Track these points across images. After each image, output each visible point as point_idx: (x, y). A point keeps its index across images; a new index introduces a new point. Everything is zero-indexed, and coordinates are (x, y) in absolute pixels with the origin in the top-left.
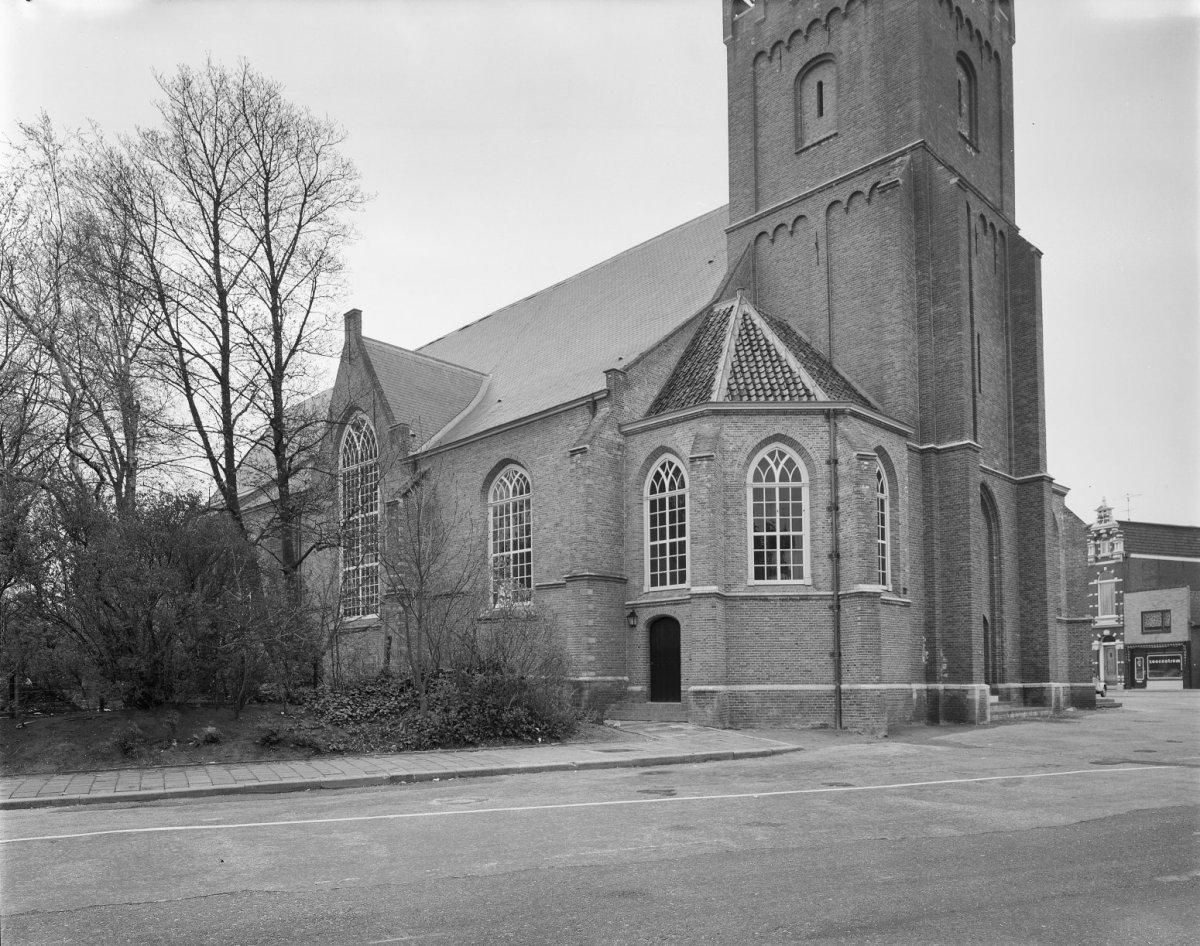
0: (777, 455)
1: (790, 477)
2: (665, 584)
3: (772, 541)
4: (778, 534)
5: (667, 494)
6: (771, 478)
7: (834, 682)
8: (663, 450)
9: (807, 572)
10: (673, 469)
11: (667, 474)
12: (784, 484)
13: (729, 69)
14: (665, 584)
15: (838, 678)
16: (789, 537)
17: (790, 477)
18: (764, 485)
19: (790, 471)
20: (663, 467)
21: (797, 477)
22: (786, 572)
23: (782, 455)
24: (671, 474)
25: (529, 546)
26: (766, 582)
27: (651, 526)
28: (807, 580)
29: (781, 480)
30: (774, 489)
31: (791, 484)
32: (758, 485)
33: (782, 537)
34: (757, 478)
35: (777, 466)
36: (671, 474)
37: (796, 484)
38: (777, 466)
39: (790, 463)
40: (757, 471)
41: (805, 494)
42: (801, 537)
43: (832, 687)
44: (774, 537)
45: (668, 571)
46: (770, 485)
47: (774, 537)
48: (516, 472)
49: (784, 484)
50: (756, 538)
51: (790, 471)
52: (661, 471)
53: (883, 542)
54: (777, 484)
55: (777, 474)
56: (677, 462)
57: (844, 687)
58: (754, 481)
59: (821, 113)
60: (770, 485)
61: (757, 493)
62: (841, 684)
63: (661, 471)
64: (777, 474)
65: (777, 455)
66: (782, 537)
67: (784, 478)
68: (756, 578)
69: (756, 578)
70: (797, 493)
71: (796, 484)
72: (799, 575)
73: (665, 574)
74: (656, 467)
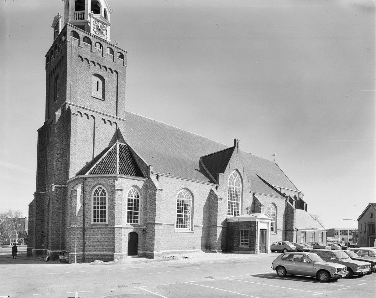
2: (99, 222)
4: (100, 210)
5: (100, 196)
6: (98, 195)
7: (83, 252)
9: (107, 220)
10: (102, 190)
11: (100, 191)
12: (102, 196)
14: (99, 222)
15: (83, 251)
18: (96, 197)
20: (98, 188)
21: (105, 195)
22: (102, 221)
23: (101, 188)
24: (101, 191)
25: (229, 202)
28: (139, 224)
29: (101, 195)
30: (99, 198)
31: (103, 196)
32: (95, 197)
33: (132, 210)
34: (95, 195)
36: (101, 191)
37: (105, 196)
39: (103, 191)
43: (82, 253)
44: (101, 209)
45: (100, 218)
46: (98, 197)
47: (101, 209)
49: (102, 196)
52: (98, 189)
53: (178, 213)
55: (100, 193)
56: (103, 188)
57: (82, 253)
59: (98, 90)
60: (98, 197)
61: (95, 199)
62: (83, 254)
63: (98, 189)
64: (100, 193)
65: (100, 188)
66: (132, 210)
67: (102, 195)
68: (94, 222)
71: (105, 196)
73: (134, 219)
74: (96, 188)
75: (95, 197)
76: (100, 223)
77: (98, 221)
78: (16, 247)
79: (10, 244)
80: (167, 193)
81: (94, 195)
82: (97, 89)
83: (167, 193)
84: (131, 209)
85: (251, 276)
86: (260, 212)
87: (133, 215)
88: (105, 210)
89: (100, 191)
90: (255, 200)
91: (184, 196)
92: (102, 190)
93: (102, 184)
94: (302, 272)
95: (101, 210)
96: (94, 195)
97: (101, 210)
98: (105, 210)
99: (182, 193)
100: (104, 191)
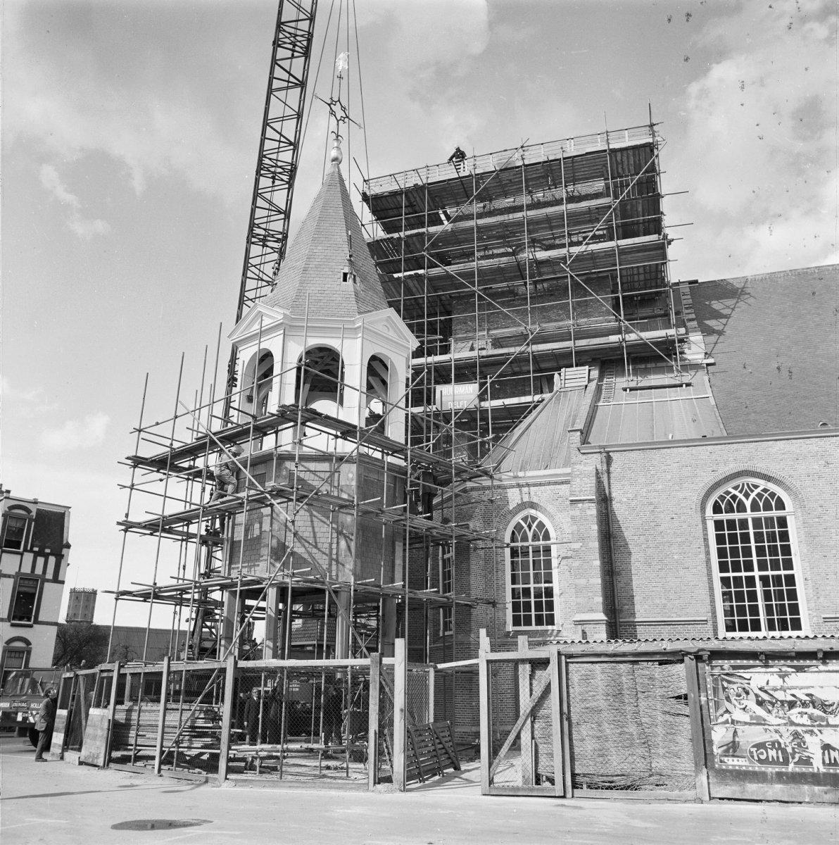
0: (529, 519)
2: (531, 625)
3: (526, 592)
6: (525, 539)
8: (533, 505)
10: (536, 523)
11: (530, 527)
12: (757, 514)
14: (531, 625)
16: (745, 571)
19: (519, 533)
20: (525, 519)
21: (547, 537)
27: (787, 532)
28: (806, 630)
29: (533, 540)
30: (746, 520)
32: (719, 517)
35: (530, 529)
38: (530, 529)
44: (760, 569)
47: (760, 569)
48: (756, 487)
49: (757, 514)
50: (513, 590)
51: (519, 533)
54: (749, 515)
55: (530, 535)
64: (530, 535)
65: (529, 519)
66: (752, 570)
67: (535, 537)
69: (514, 625)
71: (780, 513)
75: (719, 517)
76: (534, 627)
77: (528, 623)
80: (651, 508)
81: (715, 512)
82: (28, 629)
83: (651, 508)
85: (115, 827)
86: (261, 658)
87: (533, 613)
88: (550, 585)
89: (530, 527)
91: (735, 506)
92: (536, 523)
95: (537, 585)
96: (715, 512)
97: (537, 585)
98: (550, 585)
100: (544, 526)
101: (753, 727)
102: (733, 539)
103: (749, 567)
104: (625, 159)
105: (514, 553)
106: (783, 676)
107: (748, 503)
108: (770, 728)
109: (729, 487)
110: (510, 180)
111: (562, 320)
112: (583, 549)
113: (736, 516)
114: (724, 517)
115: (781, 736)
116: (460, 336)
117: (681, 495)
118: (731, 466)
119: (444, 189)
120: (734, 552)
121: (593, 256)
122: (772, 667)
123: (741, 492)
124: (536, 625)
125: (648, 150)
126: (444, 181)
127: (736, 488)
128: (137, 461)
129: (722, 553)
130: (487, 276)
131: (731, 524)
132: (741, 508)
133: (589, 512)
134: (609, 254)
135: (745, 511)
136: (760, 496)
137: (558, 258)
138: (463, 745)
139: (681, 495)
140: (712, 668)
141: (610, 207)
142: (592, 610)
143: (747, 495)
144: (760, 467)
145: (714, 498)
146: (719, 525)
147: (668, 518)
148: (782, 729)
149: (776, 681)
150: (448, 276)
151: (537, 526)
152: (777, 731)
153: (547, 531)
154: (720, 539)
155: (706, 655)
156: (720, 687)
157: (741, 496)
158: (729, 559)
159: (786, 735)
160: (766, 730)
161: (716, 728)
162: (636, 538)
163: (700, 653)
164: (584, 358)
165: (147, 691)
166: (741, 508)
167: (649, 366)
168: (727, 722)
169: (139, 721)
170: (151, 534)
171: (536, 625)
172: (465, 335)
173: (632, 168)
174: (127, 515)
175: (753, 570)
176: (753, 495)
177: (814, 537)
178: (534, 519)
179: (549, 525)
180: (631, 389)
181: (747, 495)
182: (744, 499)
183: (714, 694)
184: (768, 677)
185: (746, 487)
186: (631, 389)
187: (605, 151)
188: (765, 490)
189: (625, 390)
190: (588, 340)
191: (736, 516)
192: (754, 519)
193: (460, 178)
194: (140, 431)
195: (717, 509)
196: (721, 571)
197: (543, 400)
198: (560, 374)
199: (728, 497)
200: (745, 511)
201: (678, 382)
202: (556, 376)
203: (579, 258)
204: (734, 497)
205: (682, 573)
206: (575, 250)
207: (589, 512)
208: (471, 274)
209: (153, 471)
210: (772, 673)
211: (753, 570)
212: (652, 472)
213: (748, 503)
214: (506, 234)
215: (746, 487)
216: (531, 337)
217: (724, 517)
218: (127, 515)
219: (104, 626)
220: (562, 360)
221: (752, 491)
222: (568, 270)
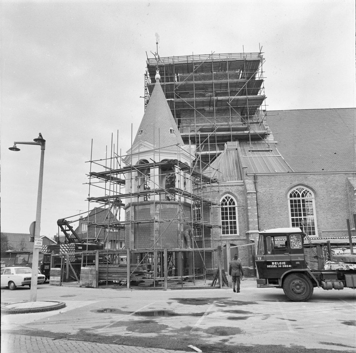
0: (228, 198)
1: (232, 204)
2: (229, 234)
4: (229, 220)
6: (226, 204)
11: (228, 200)
13: (40, 172)
14: (229, 234)
17: (232, 204)
19: (305, 194)
20: (226, 198)
21: (234, 204)
22: (231, 233)
26: (226, 235)
28: (238, 234)
29: (229, 205)
30: (300, 200)
31: (232, 206)
32: (291, 199)
39: (232, 200)
40: (291, 194)
41: (236, 208)
42: (236, 221)
44: (304, 216)
48: (303, 189)
51: (305, 194)
55: (228, 203)
56: (232, 197)
58: (290, 197)
64: (228, 203)
66: (230, 221)
67: (230, 204)
70: (234, 208)
71: (234, 206)
72: (235, 232)
75: (291, 199)
77: (227, 233)
78: (304, 249)
79: (196, 242)
80: (271, 195)
83: (271, 195)
84: (231, 223)
89: (228, 200)
90: (163, 222)
93: (229, 193)
94: (29, 142)
99: (297, 191)
101: (335, 265)
102: (296, 206)
103: (300, 215)
104: (249, 64)
105: (222, 209)
106: (344, 250)
107: (301, 195)
108: (340, 265)
109: (295, 189)
110: (206, 67)
111: (223, 122)
112: (252, 209)
113: (297, 199)
114: (293, 199)
115: (343, 267)
116: (184, 125)
117: (280, 191)
118: (296, 182)
119: (180, 67)
120: (296, 210)
121: (238, 100)
122: (340, 248)
123: (298, 191)
124: (230, 234)
125: (258, 62)
126: (181, 64)
127: (297, 189)
128: (92, 174)
129: (292, 210)
130: (198, 104)
131: (295, 201)
132: (299, 196)
133: (254, 197)
134: (245, 100)
135: (300, 197)
136: (304, 192)
137: (225, 100)
138: (209, 274)
139: (280, 191)
140: (324, 248)
141: (245, 83)
142: (255, 229)
143: (300, 192)
144: (306, 183)
145: (290, 192)
146: (291, 201)
147: (276, 199)
148: (343, 265)
149: (342, 252)
150: (183, 102)
151: (230, 200)
152: (342, 265)
153: (234, 202)
154: (292, 206)
155: (323, 245)
156: (326, 253)
157: (298, 192)
158: (294, 213)
159: (345, 266)
160: (339, 265)
161: (325, 265)
162: (266, 205)
163: (322, 244)
164: (237, 138)
165: (121, 260)
166: (299, 196)
167: (256, 142)
168: (328, 263)
169: (108, 271)
170: (97, 202)
171: (230, 234)
172: (186, 125)
173: (250, 68)
174: (89, 195)
175: (301, 216)
176: (302, 192)
177: (321, 206)
178: (229, 198)
179: (235, 200)
180: (252, 151)
181: (300, 192)
182: (299, 193)
183: (325, 255)
184: (339, 250)
185: (300, 189)
186: (252, 151)
187: (243, 61)
188: (306, 190)
189: (250, 151)
190: (237, 132)
191: (297, 199)
192: (302, 200)
193: (188, 63)
194: (91, 162)
195: (291, 196)
196: (292, 216)
197: (221, 153)
198: (226, 144)
199: (294, 192)
200: (300, 197)
201: (268, 150)
202: (225, 144)
203: (234, 100)
204: (296, 192)
205: (280, 217)
206: (233, 97)
207: (254, 197)
208: (193, 102)
209: (95, 177)
210: (341, 249)
211: (301, 216)
212: (271, 183)
213: (301, 195)
214: (205, 88)
215: (300, 189)
216: (216, 129)
217: (293, 199)
218: (89, 195)
219: (5, 233)
220: (227, 139)
221: (302, 191)
222: (230, 105)
